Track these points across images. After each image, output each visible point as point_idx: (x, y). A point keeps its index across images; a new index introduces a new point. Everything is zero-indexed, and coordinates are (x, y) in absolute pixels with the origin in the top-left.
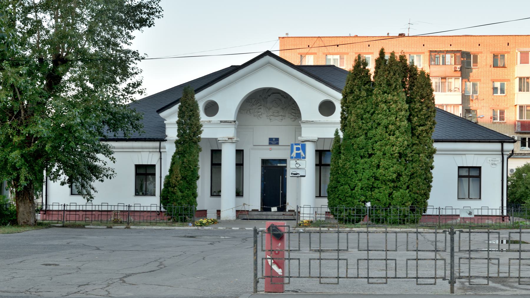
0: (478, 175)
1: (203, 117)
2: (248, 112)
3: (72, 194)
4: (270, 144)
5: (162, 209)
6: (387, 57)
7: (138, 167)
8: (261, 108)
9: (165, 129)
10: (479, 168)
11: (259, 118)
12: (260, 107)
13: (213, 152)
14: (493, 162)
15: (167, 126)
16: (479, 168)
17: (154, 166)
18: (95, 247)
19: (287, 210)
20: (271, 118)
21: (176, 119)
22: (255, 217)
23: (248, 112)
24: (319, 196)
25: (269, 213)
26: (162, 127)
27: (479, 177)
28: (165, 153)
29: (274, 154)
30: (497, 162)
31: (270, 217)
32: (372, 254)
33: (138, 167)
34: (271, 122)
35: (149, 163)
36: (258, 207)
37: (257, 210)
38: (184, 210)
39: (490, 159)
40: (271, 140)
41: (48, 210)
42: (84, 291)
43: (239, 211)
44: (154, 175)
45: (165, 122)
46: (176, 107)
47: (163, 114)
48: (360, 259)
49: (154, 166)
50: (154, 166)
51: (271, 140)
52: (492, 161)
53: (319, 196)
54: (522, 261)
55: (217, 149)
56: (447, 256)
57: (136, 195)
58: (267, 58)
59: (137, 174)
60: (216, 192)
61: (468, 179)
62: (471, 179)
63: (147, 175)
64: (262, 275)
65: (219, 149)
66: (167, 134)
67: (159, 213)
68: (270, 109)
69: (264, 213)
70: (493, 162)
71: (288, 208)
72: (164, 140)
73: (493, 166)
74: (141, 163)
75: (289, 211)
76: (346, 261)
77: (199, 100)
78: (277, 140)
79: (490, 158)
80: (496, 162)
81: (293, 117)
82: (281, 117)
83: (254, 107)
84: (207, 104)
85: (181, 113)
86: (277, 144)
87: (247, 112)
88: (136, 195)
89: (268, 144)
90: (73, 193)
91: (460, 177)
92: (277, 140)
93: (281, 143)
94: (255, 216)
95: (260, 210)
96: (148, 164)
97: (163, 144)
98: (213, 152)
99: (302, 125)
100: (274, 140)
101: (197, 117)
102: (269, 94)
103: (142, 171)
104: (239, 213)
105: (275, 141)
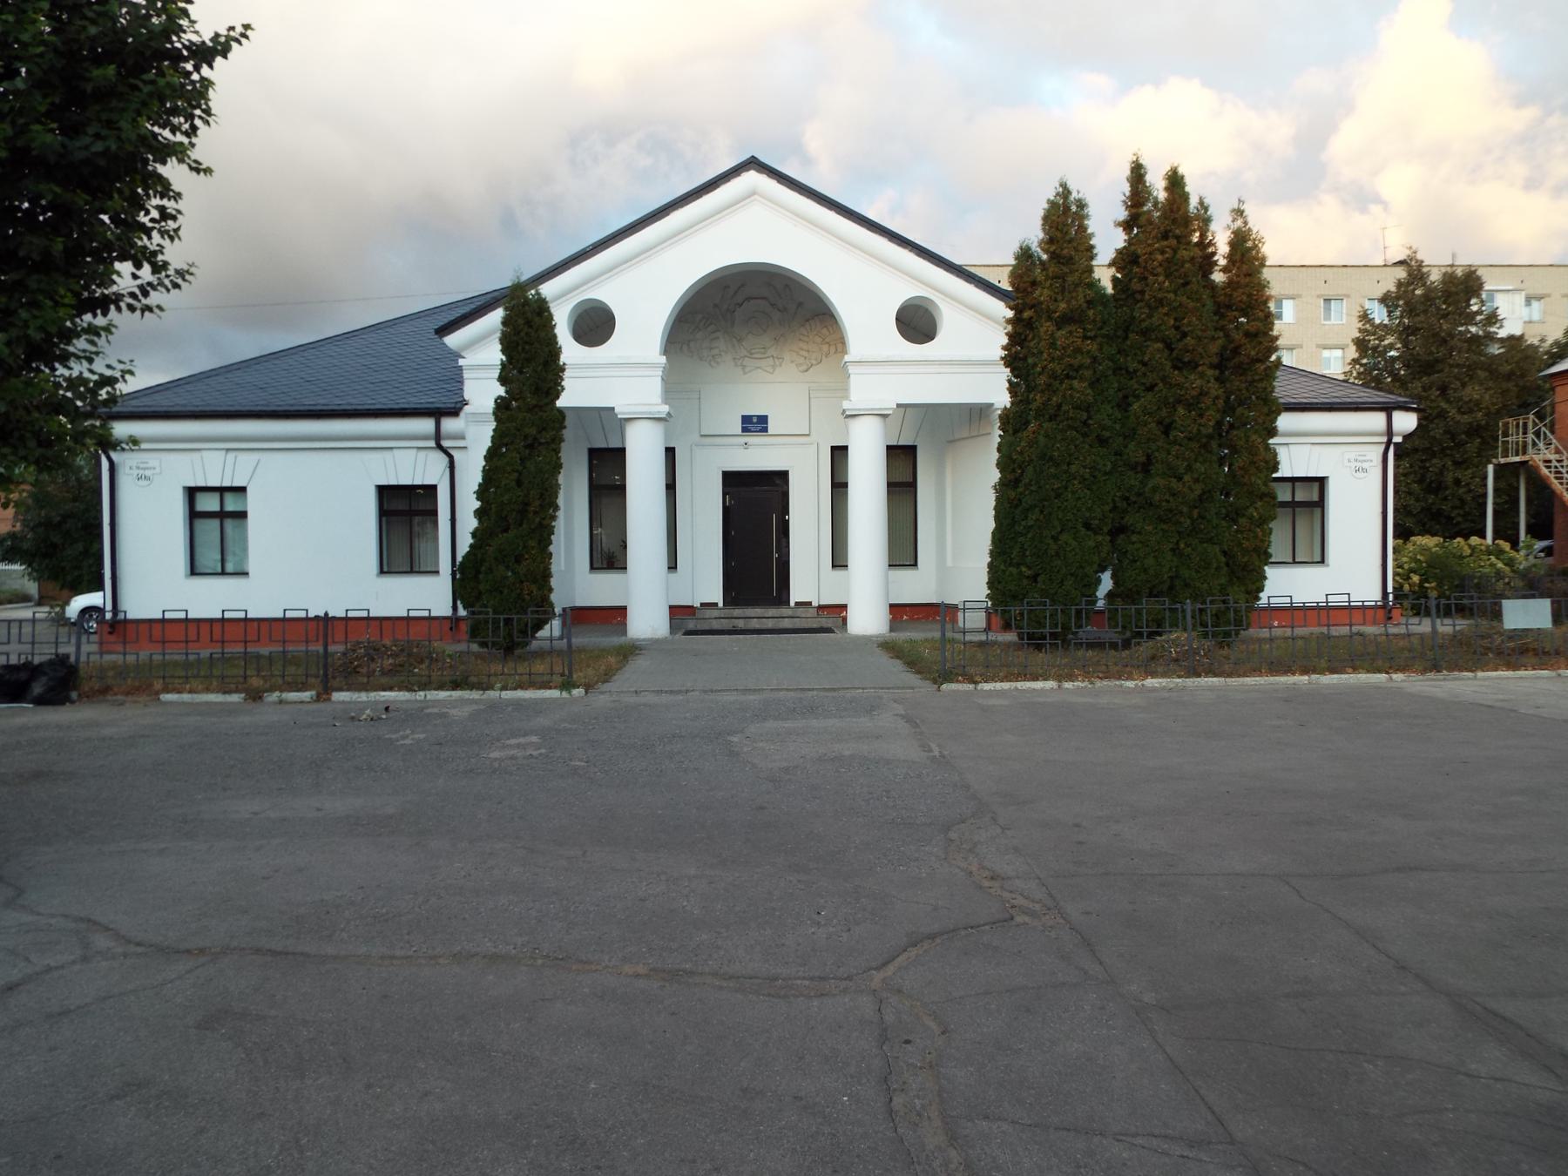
0: (1315, 498)
1: (571, 351)
2: (685, 347)
3: (194, 571)
4: (745, 430)
5: (462, 612)
7: (383, 491)
9: (461, 382)
10: (1321, 482)
11: (712, 363)
12: (718, 334)
13: (594, 453)
14: (1359, 464)
16: (1321, 482)
17: (434, 488)
19: (792, 604)
20: (744, 363)
21: (494, 355)
22: (716, 625)
23: (685, 347)
25: (784, 611)
27: (1320, 504)
29: (757, 457)
31: (786, 624)
32: (240, 649)
33: (383, 491)
36: (716, 594)
39: (1352, 456)
40: (746, 419)
41: (120, 622)
44: (434, 513)
45: (461, 362)
46: (498, 315)
47: (453, 340)
48: (211, 637)
50: (434, 488)
51: (746, 419)
52: (1356, 460)
54: (184, 651)
55: (604, 445)
57: (382, 572)
58: (752, 178)
59: (384, 513)
61: (1290, 510)
64: (332, 624)
65: (614, 444)
66: (466, 397)
69: (737, 612)
70: (1359, 464)
71: (796, 595)
72: (454, 412)
74: (393, 482)
75: (797, 603)
78: (763, 419)
79: (1352, 452)
80: (1365, 465)
81: (802, 360)
85: (510, 343)
86: (765, 430)
88: (382, 572)
89: (739, 431)
91: (194, 515)
92: (763, 419)
93: (772, 427)
94: (714, 622)
95: (721, 604)
96: (415, 483)
97: (449, 425)
98: (594, 453)
99: (852, 369)
100: (755, 420)
101: (554, 351)
103: (401, 505)
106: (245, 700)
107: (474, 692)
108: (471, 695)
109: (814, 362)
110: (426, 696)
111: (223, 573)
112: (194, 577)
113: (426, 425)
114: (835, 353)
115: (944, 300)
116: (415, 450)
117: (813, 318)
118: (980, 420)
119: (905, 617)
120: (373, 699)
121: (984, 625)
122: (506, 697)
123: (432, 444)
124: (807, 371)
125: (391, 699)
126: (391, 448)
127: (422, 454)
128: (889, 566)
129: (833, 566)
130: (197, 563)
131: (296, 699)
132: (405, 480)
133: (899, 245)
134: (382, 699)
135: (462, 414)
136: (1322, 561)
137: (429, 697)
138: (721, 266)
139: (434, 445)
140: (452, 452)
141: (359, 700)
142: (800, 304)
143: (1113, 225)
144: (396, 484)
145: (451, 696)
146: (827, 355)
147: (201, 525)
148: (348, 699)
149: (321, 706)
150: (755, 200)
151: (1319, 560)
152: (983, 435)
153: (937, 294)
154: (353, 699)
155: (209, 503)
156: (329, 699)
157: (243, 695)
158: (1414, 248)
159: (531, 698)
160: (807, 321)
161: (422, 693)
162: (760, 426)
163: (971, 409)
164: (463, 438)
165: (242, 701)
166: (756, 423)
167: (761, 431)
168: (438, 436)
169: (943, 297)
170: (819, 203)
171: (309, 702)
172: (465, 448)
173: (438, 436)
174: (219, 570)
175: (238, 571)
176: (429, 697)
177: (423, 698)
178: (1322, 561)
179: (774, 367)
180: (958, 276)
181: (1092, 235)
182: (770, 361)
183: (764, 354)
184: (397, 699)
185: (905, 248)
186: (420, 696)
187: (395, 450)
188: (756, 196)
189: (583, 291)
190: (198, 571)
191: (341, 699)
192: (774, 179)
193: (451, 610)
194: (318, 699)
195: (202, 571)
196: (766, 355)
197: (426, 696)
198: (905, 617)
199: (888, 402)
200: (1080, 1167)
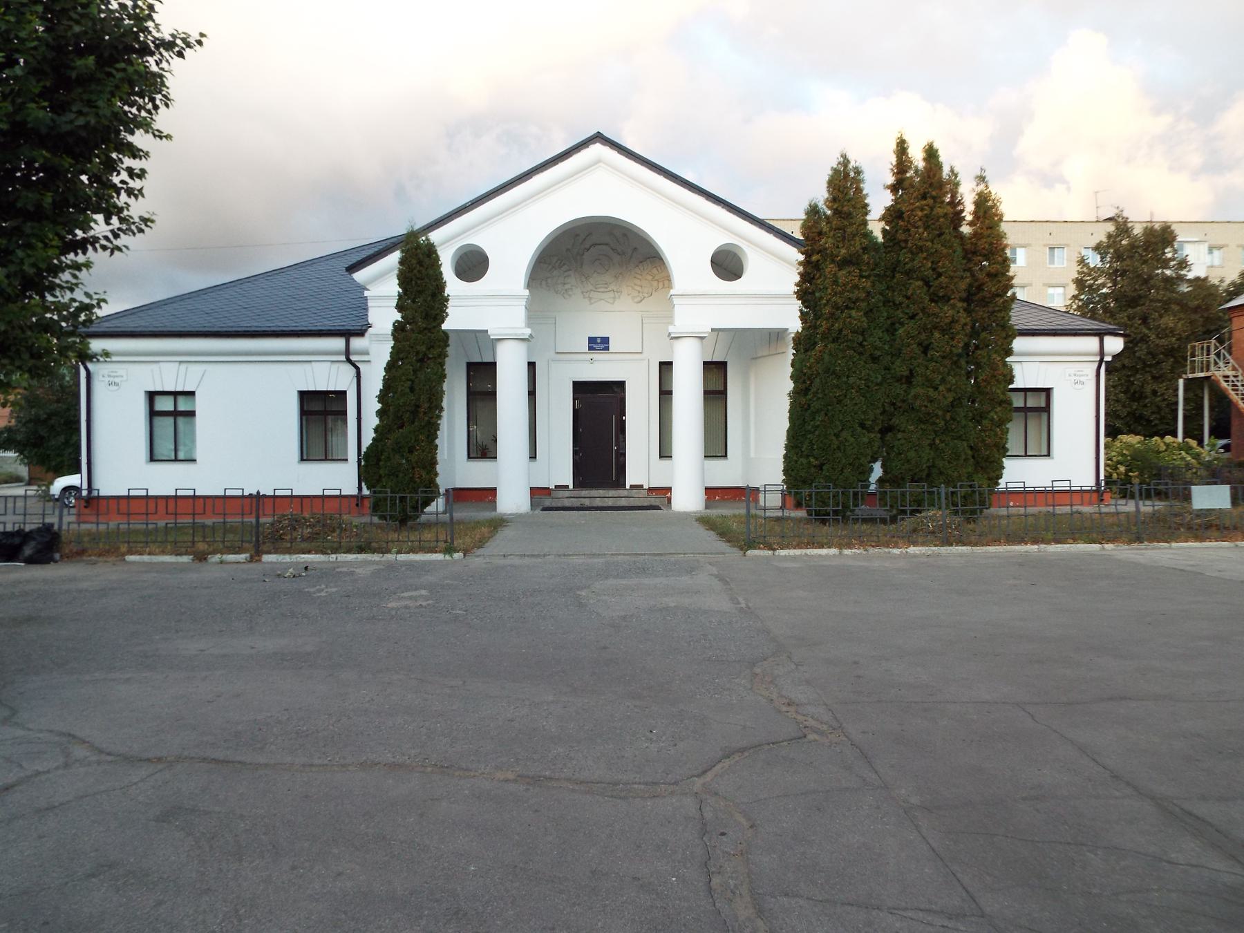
0: (1043, 405)
1: (453, 285)
2: (544, 283)
3: (152, 458)
4: (590, 348)
5: (366, 492)
7: (305, 396)
8: (569, 276)
9: (366, 309)
10: (1047, 392)
15: (370, 304)
16: (1047, 392)
17: (344, 393)
19: (628, 487)
21: (392, 288)
22: (567, 503)
23: (544, 283)
25: (621, 492)
26: (362, 307)
27: (1047, 409)
28: (368, 363)
29: (600, 370)
30: (1086, 378)
31: (623, 502)
33: (305, 396)
34: (591, 304)
36: (567, 478)
37: (567, 487)
38: (942, 378)
40: (592, 340)
41: (94, 498)
43: (546, 491)
44: (343, 413)
45: (366, 293)
47: (360, 276)
49: (342, 395)
50: (344, 393)
51: (592, 340)
52: (1075, 375)
58: (597, 149)
59: (304, 413)
60: (483, 448)
63: (325, 413)
67: (359, 499)
68: (587, 278)
69: (584, 493)
71: (631, 479)
73: (1078, 386)
75: (631, 486)
76: (202, 512)
77: (442, 244)
78: (605, 340)
80: (1082, 379)
82: (611, 294)
83: (555, 273)
84: (466, 254)
86: (607, 348)
87: (541, 284)
88: (302, 460)
90: (155, 458)
91: (153, 414)
92: (605, 340)
93: (613, 346)
97: (356, 343)
99: (676, 301)
100: (599, 341)
101: (440, 286)
102: (587, 246)
104: (537, 493)
106: (193, 560)
109: (646, 295)
110: (337, 558)
111: (176, 460)
113: (338, 343)
115: (749, 246)
116: (329, 363)
119: (717, 497)
123: (343, 358)
125: (310, 560)
126: (310, 361)
127: (336, 365)
129: (660, 457)
131: (233, 560)
134: (303, 560)
135: (367, 335)
137: (339, 559)
141: (284, 561)
142: (635, 249)
144: (314, 389)
147: (158, 421)
150: (600, 166)
153: (744, 242)
155: (165, 404)
156: (260, 560)
160: (641, 262)
161: (334, 556)
162: (603, 346)
164: (367, 353)
165: (191, 561)
168: (347, 352)
169: (747, 243)
170: (650, 169)
173: (347, 352)
174: (173, 458)
176: (339, 559)
178: (1048, 455)
185: (718, 205)
187: (313, 363)
188: (601, 164)
189: (476, 231)
191: (270, 560)
192: (615, 150)
194: (251, 560)
197: (337, 558)
198: (717, 497)
199: (705, 327)
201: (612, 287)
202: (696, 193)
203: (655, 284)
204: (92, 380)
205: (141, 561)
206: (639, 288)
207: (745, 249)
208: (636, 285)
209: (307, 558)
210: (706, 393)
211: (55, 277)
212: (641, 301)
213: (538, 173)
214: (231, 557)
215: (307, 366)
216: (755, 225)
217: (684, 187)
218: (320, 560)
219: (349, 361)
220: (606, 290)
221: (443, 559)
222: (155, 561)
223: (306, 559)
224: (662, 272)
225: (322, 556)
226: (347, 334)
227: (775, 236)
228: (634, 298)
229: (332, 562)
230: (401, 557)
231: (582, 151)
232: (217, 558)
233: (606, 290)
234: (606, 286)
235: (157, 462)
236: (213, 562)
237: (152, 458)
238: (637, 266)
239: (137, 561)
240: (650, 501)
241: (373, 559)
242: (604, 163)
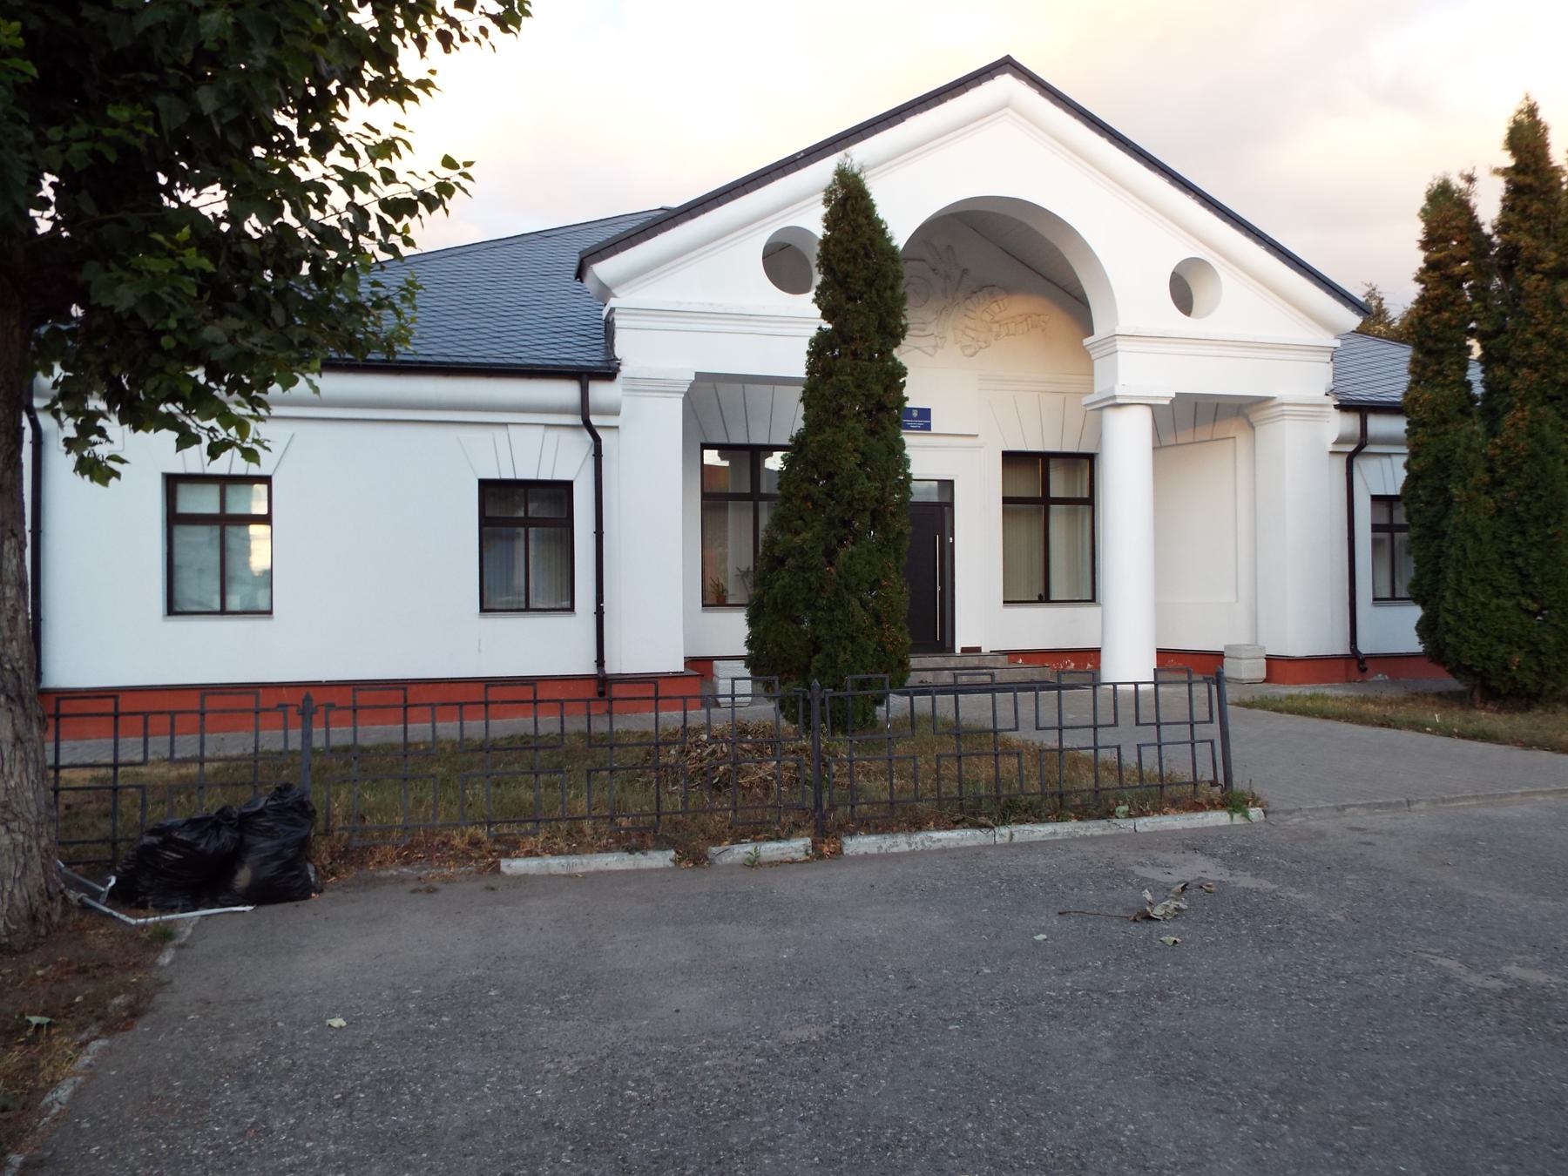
6: (393, 154)
17: (568, 485)
18: (201, 1000)
19: (958, 650)
24: (714, 598)
28: (616, 430)
35: (545, 476)
42: (1366, 1121)
47: (603, 270)
49: (564, 489)
50: (568, 485)
53: (714, 598)
56: (1214, 731)
59: (485, 521)
61: (216, 530)
62: (532, 530)
71: (961, 642)
72: (609, 372)
74: (507, 474)
75: (964, 650)
86: (927, 427)
91: (174, 519)
93: (936, 423)
96: (540, 478)
97: (600, 392)
100: (915, 414)
105: (917, 418)
106: (676, 862)
107: (1091, 823)
108: (1088, 828)
109: (983, 345)
110: (1012, 835)
111: (223, 611)
112: (174, 617)
113: (567, 392)
114: (1007, 335)
115: (1223, 265)
116: (543, 427)
117: (980, 290)
118: (1215, 420)
119: (1089, 665)
120: (920, 847)
121: (1264, 675)
122: (1146, 829)
123: (578, 420)
124: (972, 356)
125: (952, 844)
126: (506, 424)
127: (553, 435)
128: (1004, 602)
129: (482, 610)
130: (178, 596)
131: (776, 856)
132: (527, 471)
133: (1181, 189)
134: (938, 845)
135: (619, 377)
136: (1093, 600)
137: (1017, 838)
138: (942, 207)
139: (581, 423)
140: (601, 433)
141: (895, 850)
142: (965, 271)
143: (1488, 173)
144: (498, 477)
145: (1055, 833)
146: (997, 336)
147: (183, 533)
148: (875, 851)
149: (821, 873)
150: (1006, 114)
151: (1089, 598)
152: (1217, 440)
153: (1216, 256)
154: (883, 851)
155: (202, 501)
156: (838, 852)
157: (672, 853)
158: (1374, 285)
159: (1184, 829)
160: (975, 292)
161: (1005, 831)
162: (921, 422)
163: (1196, 404)
164: (617, 413)
165: (671, 865)
166: (917, 418)
167: (923, 428)
168: (584, 409)
169: (1223, 260)
170: (1088, 126)
171: (806, 861)
172: (617, 427)
173: (584, 409)
174: (217, 607)
175: (250, 609)
176: (1017, 838)
177: (1007, 839)
178: (1093, 600)
179: (935, 347)
180: (1247, 235)
181: (1558, 170)
182: (931, 341)
183: (924, 330)
184: (963, 844)
185: (1187, 193)
186: (1001, 835)
187: (510, 427)
188: (1008, 110)
189: (807, 206)
190: (178, 609)
191: (861, 850)
192: (1034, 87)
193: (595, 665)
194: (817, 854)
195: (492, 607)
196: (926, 333)
197: (1012, 835)
198: (1089, 665)
199: (1165, 389)
200: (505, 1109)
201: (931, 329)
202: (1155, 171)
203: (995, 327)
204: (43, 447)
205: (544, 872)
206: (972, 334)
207: (1217, 269)
208: (967, 327)
209: (950, 839)
210: (1006, 500)
211: (377, 79)
212: (975, 353)
213: (915, 114)
214: (771, 850)
215: (500, 433)
216: (1239, 229)
217: (1139, 161)
218: (974, 843)
219: (587, 425)
220: (922, 334)
221: (1229, 823)
222: (580, 870)
223: (944, 843)
224: (1006, 309)
225: (978, 832)
226: (583, 375)
227: (1268, 250)
228: (963, 348)
229: (1001, 845)
230: (1145, 824)
231: (997, 78)
232: (743, 850)
233: (922, 334)
234: (923, 326)
235: (179, 617)
236: (730, 866)
237: (172, 610)
238: (969, 298)
239: (531, 872)
240: (1023, 673)
241: (1088, 834)
242: (1016, 111)
